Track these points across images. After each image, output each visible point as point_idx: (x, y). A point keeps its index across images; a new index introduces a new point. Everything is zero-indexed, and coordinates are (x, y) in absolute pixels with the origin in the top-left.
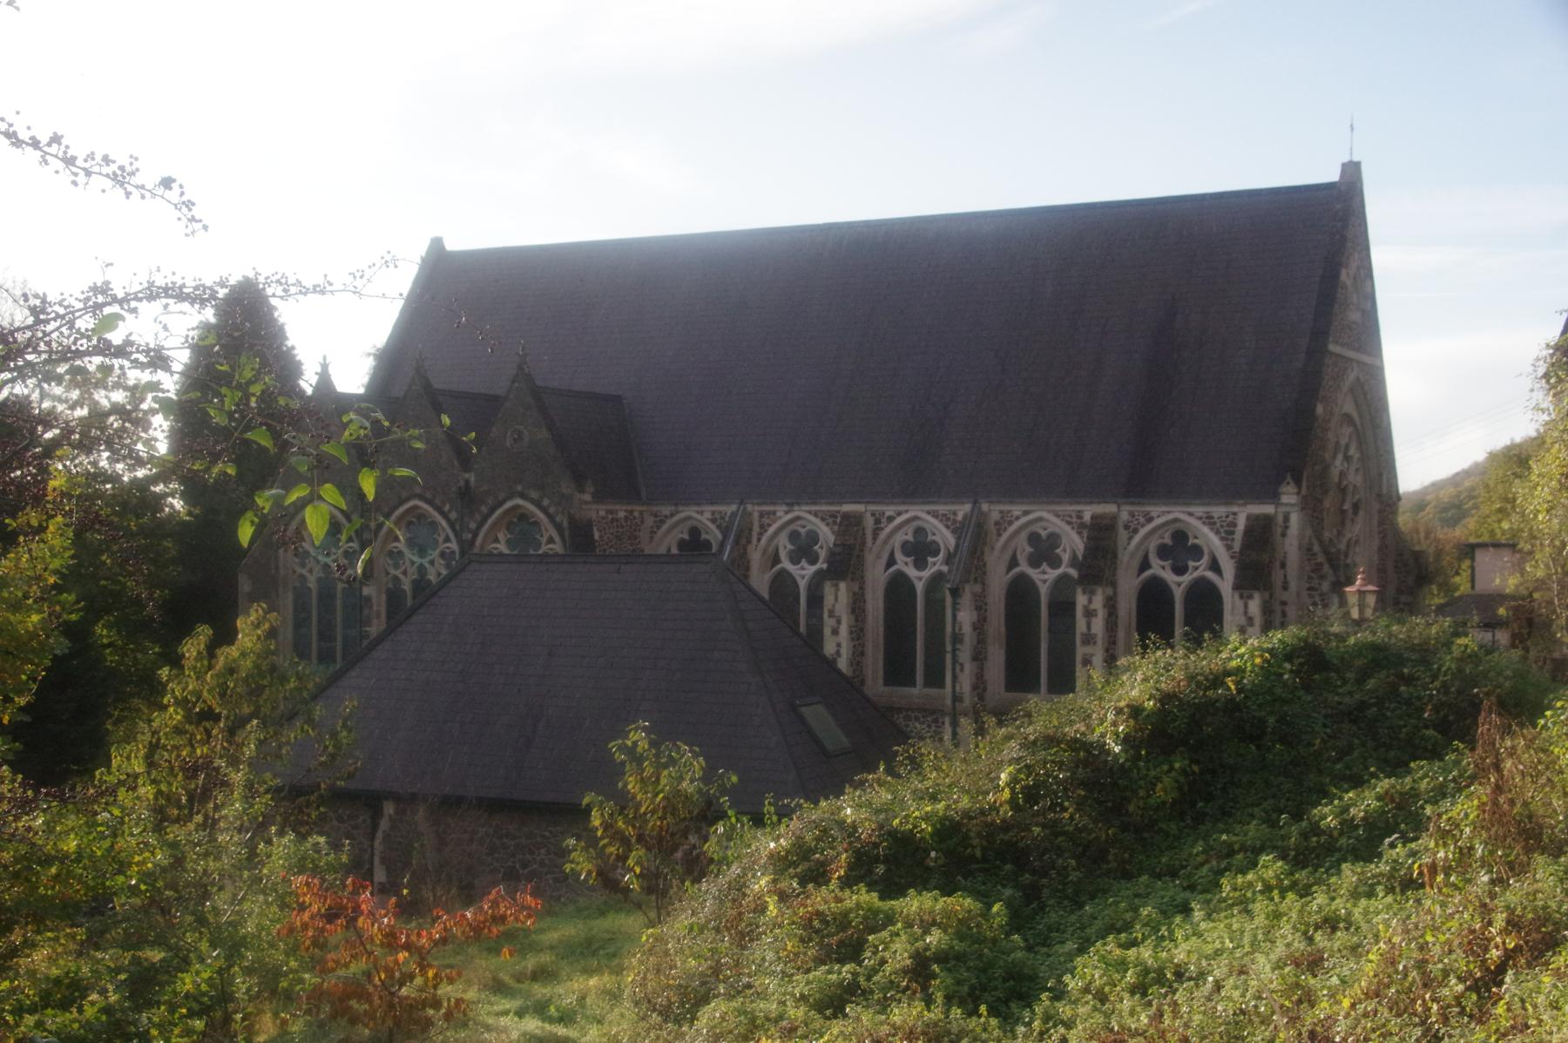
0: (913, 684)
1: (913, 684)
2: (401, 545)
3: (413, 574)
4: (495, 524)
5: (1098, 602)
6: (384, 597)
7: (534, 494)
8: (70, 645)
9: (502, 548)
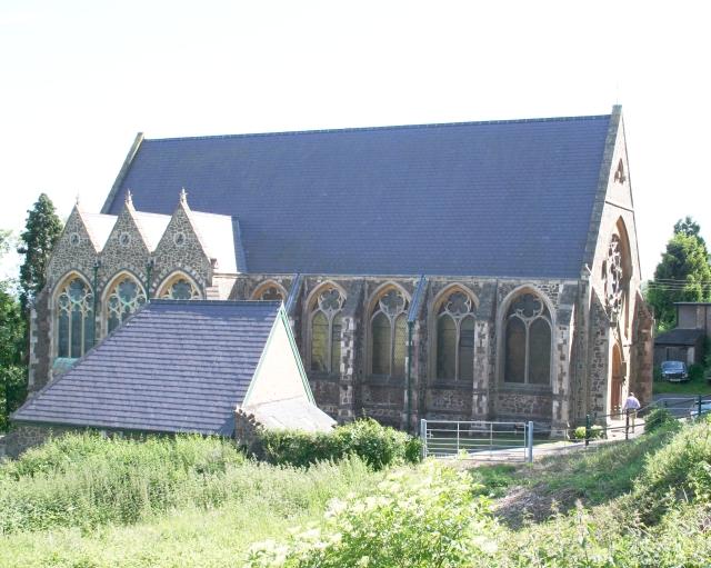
0: (522, 381)
1: (522, 381)
2: (117, 295)
3: (123, 310)
4: (112, 285)
5: (486, 329)
6: (107, 323)
7: (187, 268)
8: (648, 456)
9: (170, 297)
